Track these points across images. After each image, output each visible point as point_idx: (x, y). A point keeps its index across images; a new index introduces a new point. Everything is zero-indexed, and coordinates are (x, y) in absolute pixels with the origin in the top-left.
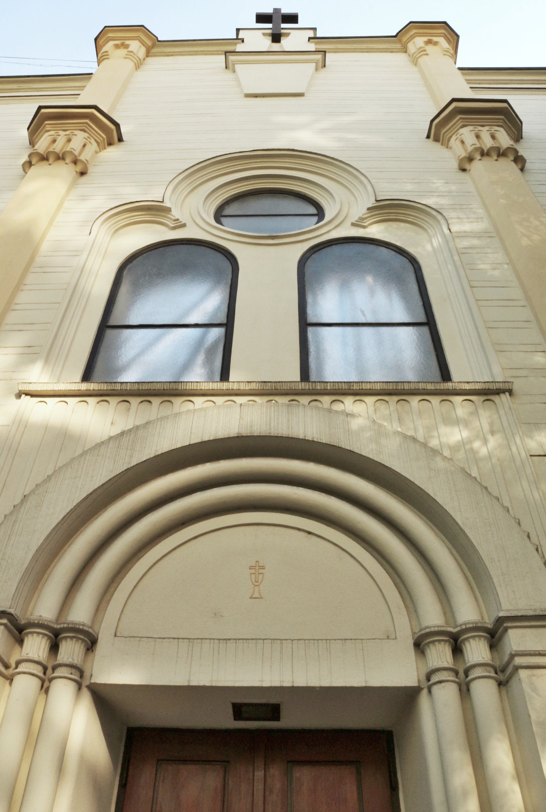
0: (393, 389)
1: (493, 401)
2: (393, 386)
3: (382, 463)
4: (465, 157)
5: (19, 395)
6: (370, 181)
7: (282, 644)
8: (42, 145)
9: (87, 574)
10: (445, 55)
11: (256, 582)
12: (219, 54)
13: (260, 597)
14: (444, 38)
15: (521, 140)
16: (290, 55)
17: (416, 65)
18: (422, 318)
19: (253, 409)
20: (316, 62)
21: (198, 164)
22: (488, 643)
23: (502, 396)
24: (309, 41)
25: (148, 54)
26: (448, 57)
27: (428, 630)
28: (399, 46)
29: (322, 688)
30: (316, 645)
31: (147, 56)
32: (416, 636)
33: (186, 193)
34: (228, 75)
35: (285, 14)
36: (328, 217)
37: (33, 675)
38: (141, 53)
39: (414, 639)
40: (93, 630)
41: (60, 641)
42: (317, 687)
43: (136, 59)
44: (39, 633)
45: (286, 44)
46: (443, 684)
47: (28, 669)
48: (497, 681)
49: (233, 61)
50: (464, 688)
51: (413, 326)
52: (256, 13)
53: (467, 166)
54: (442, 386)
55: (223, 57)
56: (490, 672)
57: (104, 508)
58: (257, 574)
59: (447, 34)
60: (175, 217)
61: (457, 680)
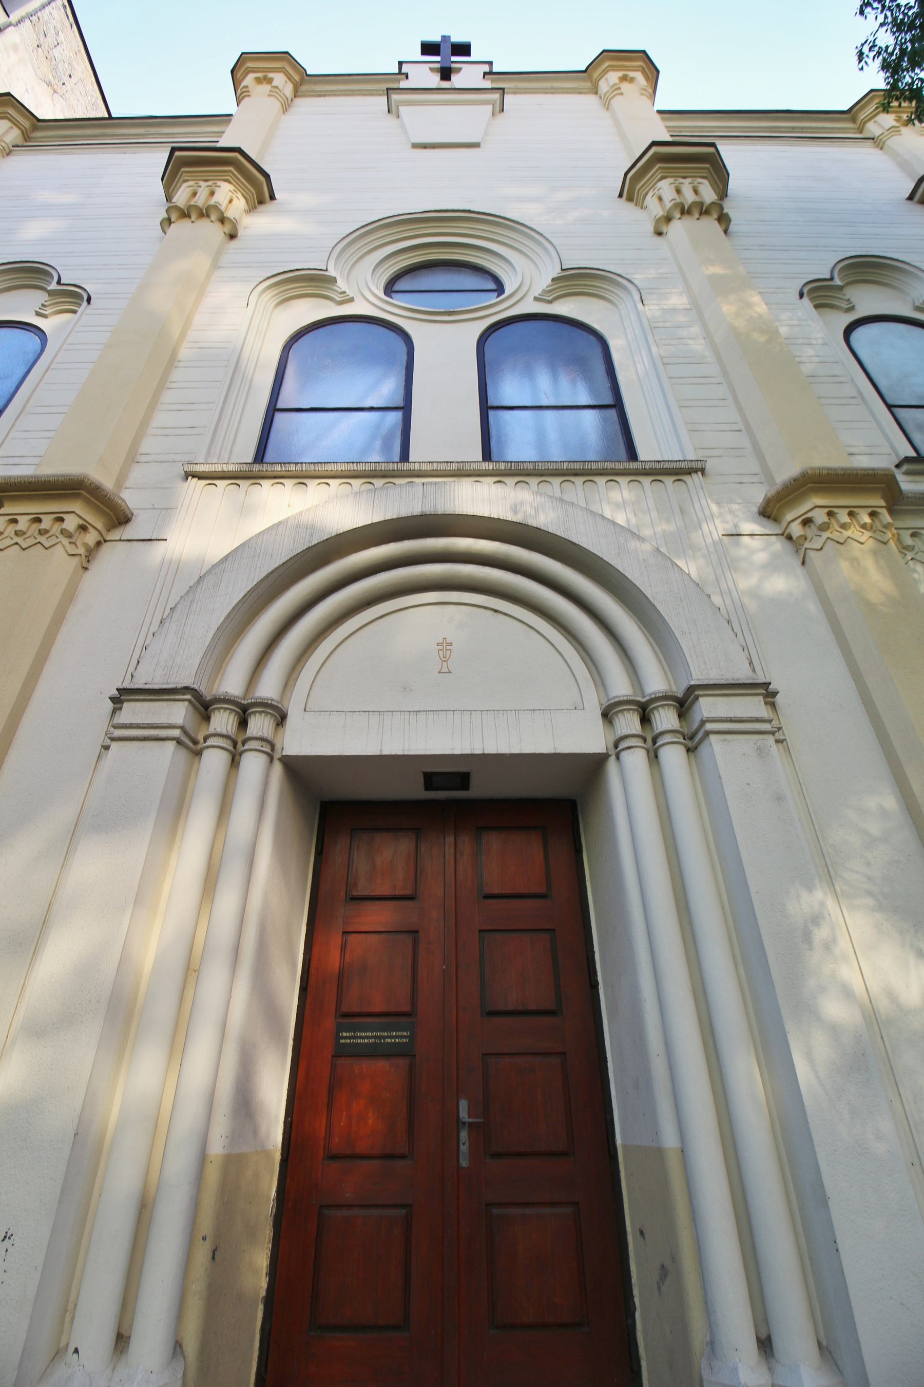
0: (580, 469)
1: (684, 482)
2: (580, 466)
3: (570, 540)
4: (663, 217)
6: (555, 247)
7: (471, 714)
8: (181, 197)
9: (273, 652)
10: (642, 94)
11: (444, 657)
12: (379, 95)
13: (448, 671)
14: (642, 72)
15: (725, 199)
16: (463, 93)
17: (608, 109)
18: (608, 400)
19: (437, 487)
20: (493, 105)
21: (363, 227)
22: (676, 711)
23: (694, 475)
24: (484, 77)
25: (296, 94)
26: (645, 97)
27: (616, 700)
28: (588, 85)
29: (512, 755)
30: (505, 715)
31: (295, 96)
32: (604, 706)
33: (352, 262)
34: (391, 120)
35: (456, 43)
36: (508, 290)
37: (222, 748)
38: (289, 90)
39: (602, 710)
40: (282, 705)
41: (249, 717)
42: (508, 754)
43: (281, 96)
44: (225, 709)
45: (457, 80)
46: (631, 750)
47: (217, 742)
48: (685, 747)
49: (396, 102)
50: (652, 754)
51: (599, 409)
52: (422, 41)
53: (664, 229)
54: (631, 465)
55: (384, 99)
56: (679, 738)
57: (286, 589)
58: (445, 644)
59: (645, 67)
60: (341, 289)
61: (645, 746)
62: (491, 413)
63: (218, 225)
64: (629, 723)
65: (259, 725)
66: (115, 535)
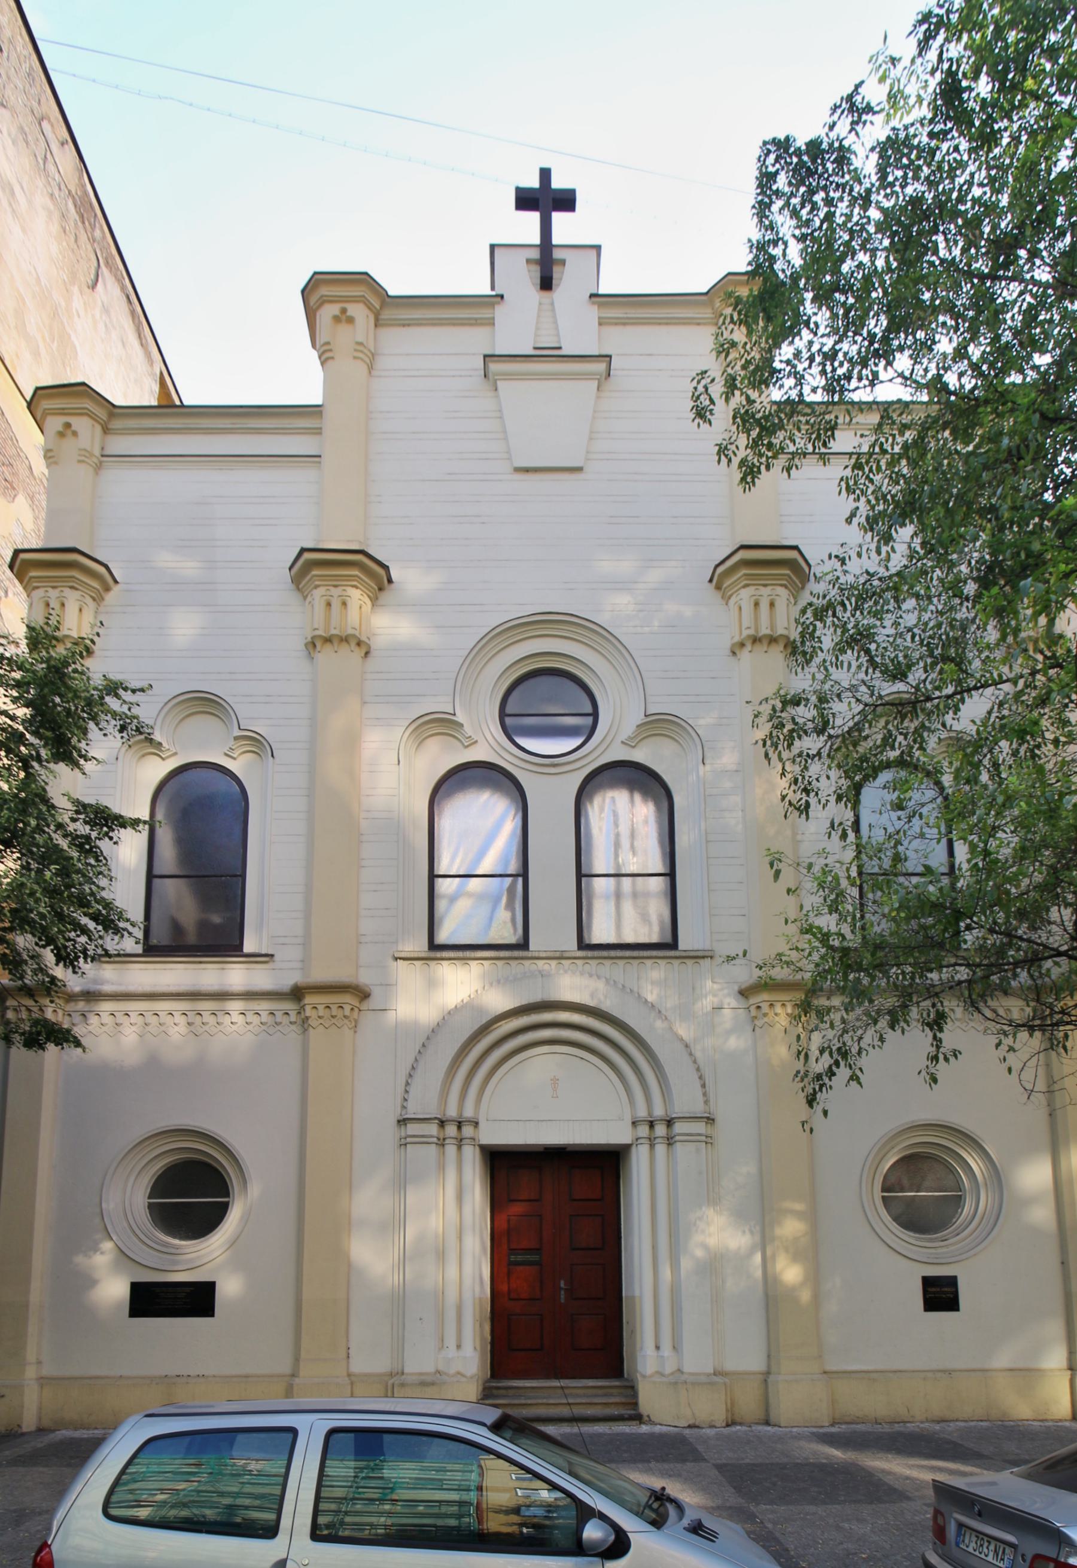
5: (396, 959)
62: (584, 880)
63: (356, 649)
64: (643, 1131)
65: (468, 1131)
66: (364, 1006)
